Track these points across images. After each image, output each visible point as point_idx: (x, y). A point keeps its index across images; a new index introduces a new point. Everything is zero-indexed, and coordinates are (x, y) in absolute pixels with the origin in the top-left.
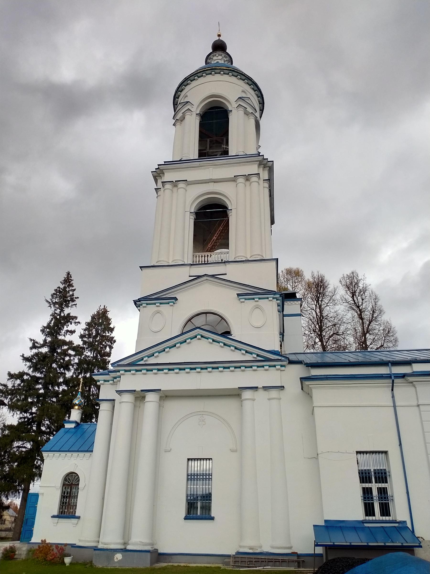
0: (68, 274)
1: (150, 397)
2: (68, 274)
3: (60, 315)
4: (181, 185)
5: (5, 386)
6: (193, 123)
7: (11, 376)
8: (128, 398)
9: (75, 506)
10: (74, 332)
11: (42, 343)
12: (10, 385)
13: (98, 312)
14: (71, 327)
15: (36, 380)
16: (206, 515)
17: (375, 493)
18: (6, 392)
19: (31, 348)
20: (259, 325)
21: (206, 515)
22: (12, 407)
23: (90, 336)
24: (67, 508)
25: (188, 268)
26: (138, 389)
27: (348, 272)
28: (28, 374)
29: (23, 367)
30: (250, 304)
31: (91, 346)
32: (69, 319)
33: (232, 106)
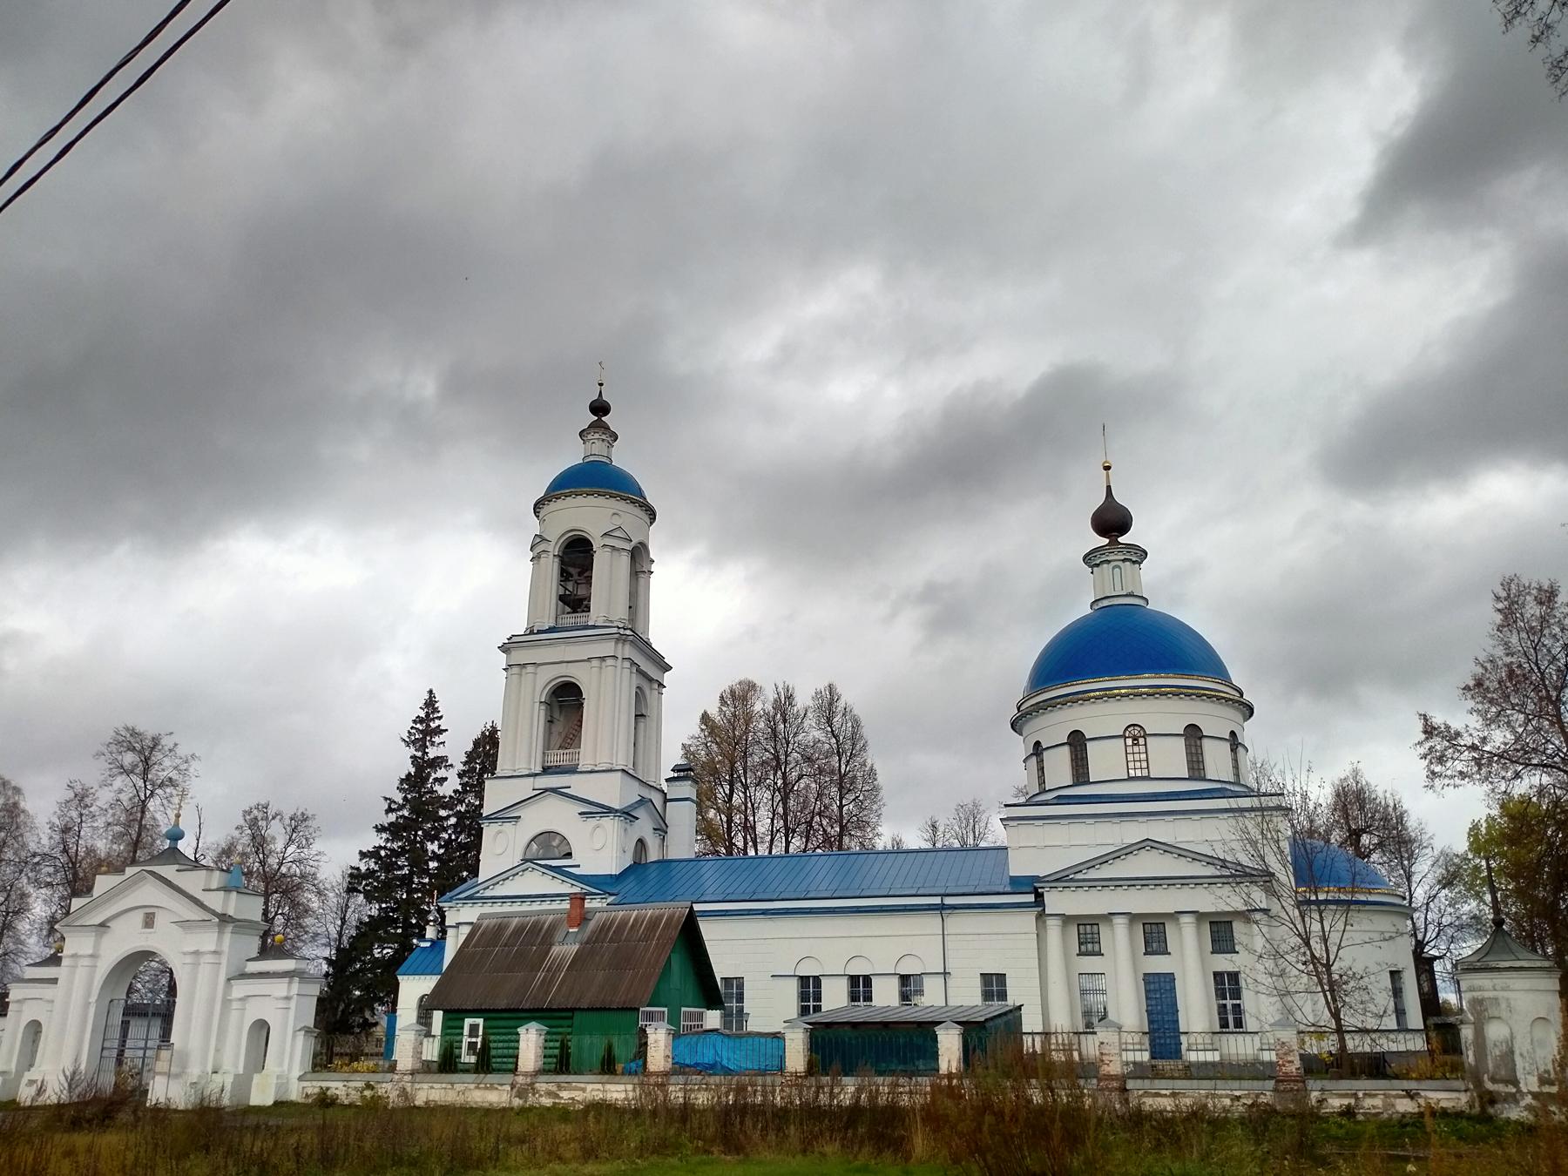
0: (431, 692)
2: (431, 692)
4: (530, 669)
6: (551, 566)
7: (363, 855)
14: (441, 773)
16: (986, 978)
21: (986, 978)
22: (369, 897)
28: (385, 848)
29: (378, 840)
30: (592, 822)
32: (439, 762)
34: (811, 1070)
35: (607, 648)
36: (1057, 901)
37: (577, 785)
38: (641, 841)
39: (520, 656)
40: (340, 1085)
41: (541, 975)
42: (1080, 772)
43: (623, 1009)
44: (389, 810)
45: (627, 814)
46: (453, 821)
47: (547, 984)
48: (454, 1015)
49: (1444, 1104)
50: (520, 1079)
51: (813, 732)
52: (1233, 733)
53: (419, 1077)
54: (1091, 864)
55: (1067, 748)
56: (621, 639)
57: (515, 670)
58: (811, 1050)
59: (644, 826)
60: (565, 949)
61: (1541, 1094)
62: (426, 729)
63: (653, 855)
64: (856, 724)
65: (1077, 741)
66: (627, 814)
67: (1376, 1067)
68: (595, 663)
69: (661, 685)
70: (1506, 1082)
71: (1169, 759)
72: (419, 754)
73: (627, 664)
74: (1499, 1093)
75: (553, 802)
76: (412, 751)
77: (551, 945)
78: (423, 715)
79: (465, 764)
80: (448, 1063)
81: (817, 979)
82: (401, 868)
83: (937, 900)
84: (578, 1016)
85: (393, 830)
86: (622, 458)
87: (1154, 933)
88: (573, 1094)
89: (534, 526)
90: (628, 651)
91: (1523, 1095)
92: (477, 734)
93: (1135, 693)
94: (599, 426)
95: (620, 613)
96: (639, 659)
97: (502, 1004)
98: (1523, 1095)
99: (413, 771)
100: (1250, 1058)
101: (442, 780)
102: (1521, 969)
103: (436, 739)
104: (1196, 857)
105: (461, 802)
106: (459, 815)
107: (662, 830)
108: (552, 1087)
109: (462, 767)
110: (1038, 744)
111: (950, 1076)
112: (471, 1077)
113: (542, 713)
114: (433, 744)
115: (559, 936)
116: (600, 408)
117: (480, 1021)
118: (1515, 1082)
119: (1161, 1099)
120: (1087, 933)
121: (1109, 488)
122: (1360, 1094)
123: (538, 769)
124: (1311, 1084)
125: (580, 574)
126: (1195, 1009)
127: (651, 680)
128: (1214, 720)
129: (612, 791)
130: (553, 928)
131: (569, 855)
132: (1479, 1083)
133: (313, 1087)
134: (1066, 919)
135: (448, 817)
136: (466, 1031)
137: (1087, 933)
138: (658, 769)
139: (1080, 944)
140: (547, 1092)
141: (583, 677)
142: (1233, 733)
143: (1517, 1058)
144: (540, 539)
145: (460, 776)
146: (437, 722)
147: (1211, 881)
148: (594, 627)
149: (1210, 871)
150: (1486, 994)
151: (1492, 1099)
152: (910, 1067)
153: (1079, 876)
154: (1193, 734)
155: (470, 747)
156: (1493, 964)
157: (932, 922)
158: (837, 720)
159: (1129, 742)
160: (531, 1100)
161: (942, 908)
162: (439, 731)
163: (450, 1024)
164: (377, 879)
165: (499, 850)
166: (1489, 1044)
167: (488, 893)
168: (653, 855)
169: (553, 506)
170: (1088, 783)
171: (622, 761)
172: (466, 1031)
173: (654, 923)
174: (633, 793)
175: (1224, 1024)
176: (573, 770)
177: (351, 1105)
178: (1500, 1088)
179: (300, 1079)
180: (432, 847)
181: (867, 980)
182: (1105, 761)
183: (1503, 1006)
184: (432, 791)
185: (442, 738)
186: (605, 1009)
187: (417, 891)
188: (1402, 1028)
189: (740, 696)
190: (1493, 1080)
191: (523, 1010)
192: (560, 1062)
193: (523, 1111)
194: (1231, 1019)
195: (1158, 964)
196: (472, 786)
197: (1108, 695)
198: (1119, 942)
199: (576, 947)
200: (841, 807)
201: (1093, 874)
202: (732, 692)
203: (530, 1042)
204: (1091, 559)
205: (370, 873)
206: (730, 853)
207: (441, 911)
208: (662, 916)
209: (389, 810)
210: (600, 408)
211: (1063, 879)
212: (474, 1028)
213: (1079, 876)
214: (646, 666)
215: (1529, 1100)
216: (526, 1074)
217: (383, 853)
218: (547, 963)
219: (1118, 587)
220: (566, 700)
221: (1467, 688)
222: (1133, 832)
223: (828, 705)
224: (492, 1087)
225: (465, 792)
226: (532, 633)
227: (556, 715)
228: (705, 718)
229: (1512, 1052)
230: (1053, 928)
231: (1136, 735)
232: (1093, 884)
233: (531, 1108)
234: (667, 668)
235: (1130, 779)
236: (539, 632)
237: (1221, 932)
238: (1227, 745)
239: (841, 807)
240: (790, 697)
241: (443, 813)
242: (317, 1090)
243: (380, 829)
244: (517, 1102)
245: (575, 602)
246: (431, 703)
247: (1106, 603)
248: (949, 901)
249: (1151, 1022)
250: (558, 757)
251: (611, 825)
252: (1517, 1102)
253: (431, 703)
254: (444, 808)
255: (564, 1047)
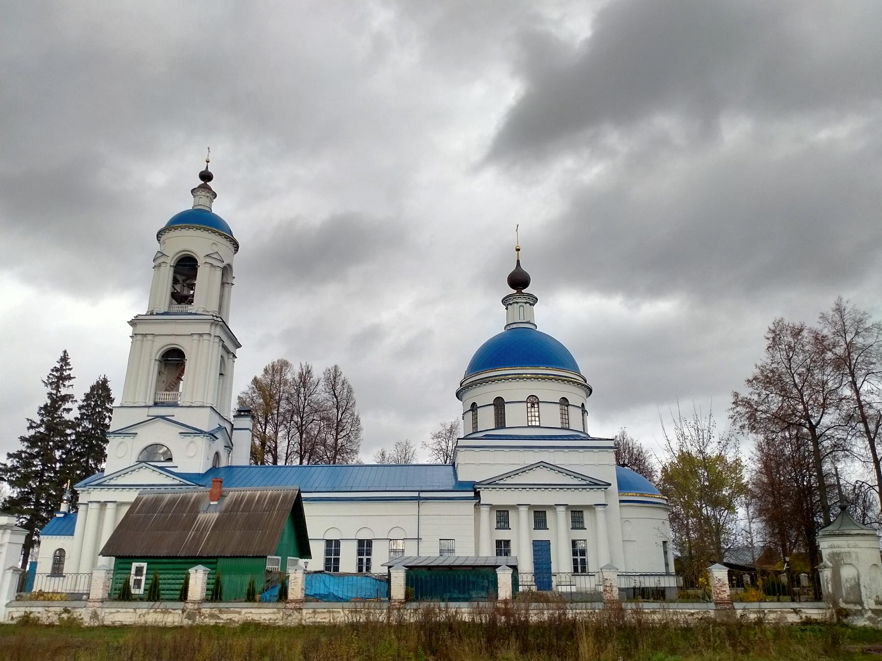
0: (65, 352)
1: (109, 505)
2: (65, 352)
3: (56, 395)
4: (149, 337)
5: (5, 465)
6: (167, 273)
7: (10, 456)
8: (95, 506)
9: (62, 569)
10: (71, 409)
11: (39, 422)
12: (9, 465)
13: (98, 382)
14: (68, 405)
15: (33, 456)
17: (365, 561)
18: (6, 470)
19: (29, 428)
20: (192, 454)
22: (12, 484)
23: (89, 405)
24: (57, 570)
25: (147, 409)
26: (102, 500)
27: (330, 365)
28: (25, 452)
29: (23, 447)
30: (188, 439)
31: (89, 418)
32: (66, 398)
33: (200, 262)
34: (408, 598)
35: (206, 328)
36: (487, 497)
37: (179, 414)
38: (217, 453)
39: (141, 329)
40: (40, 609)
41: (191, 533)
42: (500, 422)
43: (257, 557)
44: (31, 427)
45: (212, 435)
46: (73, 437)
47: (197, 540)
48: (123, 560)
49: (816, 617)
50: (190, 606)
51: (321, 394)
52: (583, 404)
53: (107, 604)
54: (508, 475)
55: (493, 407)
56: (214, 323)
57: (139, 337)
58: (407, 584)
59: (219, 445)
60: (209, 515)
61: (876, 610)
62: (60, 375)
63: (223, 463)
64: (350, 391)
65: (499, 404)
66: (212, 435)
67: (659, 594)
68: (196, 337)
69: (234, 356)
70: (855, 603)
71: (551, 416)
72: (54, 392)
73: (217, 340)
74: (851, 610)
75: (161, 425)
76: (49, 389)
77: (198, 512)
78: (58, 366)
79: (84, 401)
80: (123, 595)
81: (337, 542)
82: (36, 466)
83: (416, 494)
84: (221, 562)
85: (32, 441)
86: (218, 208)
87: (540, 517)
88: (230, 616)
89: (156, 246)
90: (218, 331)
91: (866, 611)
92: (93, 382)
93: (536, 377)
94: (205, 187)
95: (214, 307)
96: (224, 338)
97: (164, 553)
98: (866, 611)
99: (49, 402)
100: (583, 590)
101: (68, 410)
102: (864, 534)
103: (67, 383)
104: (569, 473)
105: (79, 425)
106: (77, 433)
107: (229, 447)
108: (214, 611)
109: (81, 403)
110: (474, 404)
111: (505, 602)
112: (145, 604)
113: (156, 367)
114: (64, 385)
115: (203, 507)
116: (206, 176)
117: (145, 565)
118: (861, 603)
119: (536, 615)
120: (503, 516)
121: (518, 261)
122: (766, 611)
123: (151, 403)
124: (737, 605)
125: (184, 281)
126: (561, 561)
127: (228, 352)
128: (575, 396)
129: (204, 420)
130: (198, 501)
131: (170, 459)
132: (835, 604)
133: (18, 612)
134: (492, 507)
135: (70, 435)
136: (133, 571)
137: (503, 516)
138: (229, 410)
139: (498, 522)
140: (215, 615)
141: (185, 345)
142: (583, 404)
143: (863, 589)
144: (161, 254)
145: (80, 408)
146: (68, 372)
147: (576, 487)
148: (196, 314)
149: (576, 481)
150: (842, 550)
151: (843, 613)
152: (466, 596)
153: (501, 482)
154: (564, 402)
155: (88, 391)
156: (847, 532)
157: (412, 507)
158: (339, 387)
159: (529, 405)
160: (198, 620)
161: (418, 499)
162: (69, 378)
163: (121, 566)
164: (19, 472)
165: (118, 455)
166: (843, 580)
167: (112, 482)
168: (223, 463)
169: (172, 234)
170: (504, 427)
171: (209, 402)
172: (133, 571)
173: (274, 500)
174: (215, 422)
175: (576, 569)
176: (175, 405)
177: (51, 625)
178: (851, 607)
179: (7, 606)
180: (58, 454)
181: (369, 543)
182: (515, 415)
183: (854, 556)
184: (61, 417)
185: (71, 382)
186: (243, 557)
187: (46, 481)
188: (668, 574)
189: (278, 369)
190: (846, 602)
191: (180, 557)
192: (215, 594)
193: (191, 628)
194: (580, 566)
195: (541, 535)
196: (88, 416)
197: (519, 377)
198: (522, 522)
199: (217, 515)
200: (336, 440)
201: (509, 481)
202: (273, 366)
203: (198, 580)
204: (506, 301)
205: (14, 469)
206: (275, 462)
207: (75, 494)
208: (279, 496)
209: (31, 427)
210: (206, 176)
211: (492, 484)
212: (139, 571)
213: (501, 482)
214: (228, 344)
215: (869, 614)
216: (194, 602)
217: (23, 455)
218: (195, 525)
219: (522, 318)
220: (173, 361)
221: (749, 381)
222: (532, 457)
223: (334, 379)
224: (166, 611)
225: (82, 419)
226: (152, 314)
227: (163, 370)
228: (255, 381)
229: (859, 585)
230: (485, 511)
231: (533, 401)
232: (510, 487)
233: (199, 627)
234: (238, 346)
235: (529, 426)
236: (157, 314)
237: (577, 516)
238: (580, 411)
239: (336, 440)
240: (309, 372)
241: (68, 431)
242: (22, 614)
243: (23, 439)
244: (186, 622)
245: (181, 298)
246: (64, 359)
247: (515, 326)
248: (423, 495)
249: (536, 569)
250: (167, 397)
251: (201, 442)
252: (862, 615)
253: (64, 359)
254: (69, 428)
255: (218, 583)
